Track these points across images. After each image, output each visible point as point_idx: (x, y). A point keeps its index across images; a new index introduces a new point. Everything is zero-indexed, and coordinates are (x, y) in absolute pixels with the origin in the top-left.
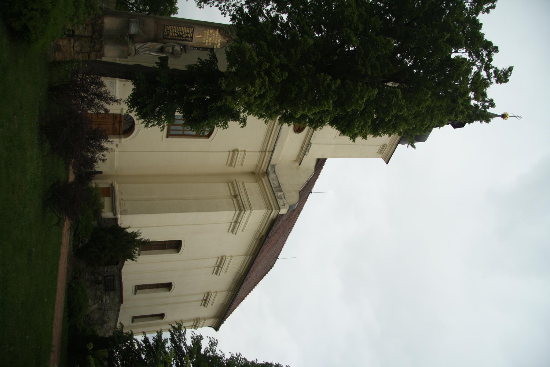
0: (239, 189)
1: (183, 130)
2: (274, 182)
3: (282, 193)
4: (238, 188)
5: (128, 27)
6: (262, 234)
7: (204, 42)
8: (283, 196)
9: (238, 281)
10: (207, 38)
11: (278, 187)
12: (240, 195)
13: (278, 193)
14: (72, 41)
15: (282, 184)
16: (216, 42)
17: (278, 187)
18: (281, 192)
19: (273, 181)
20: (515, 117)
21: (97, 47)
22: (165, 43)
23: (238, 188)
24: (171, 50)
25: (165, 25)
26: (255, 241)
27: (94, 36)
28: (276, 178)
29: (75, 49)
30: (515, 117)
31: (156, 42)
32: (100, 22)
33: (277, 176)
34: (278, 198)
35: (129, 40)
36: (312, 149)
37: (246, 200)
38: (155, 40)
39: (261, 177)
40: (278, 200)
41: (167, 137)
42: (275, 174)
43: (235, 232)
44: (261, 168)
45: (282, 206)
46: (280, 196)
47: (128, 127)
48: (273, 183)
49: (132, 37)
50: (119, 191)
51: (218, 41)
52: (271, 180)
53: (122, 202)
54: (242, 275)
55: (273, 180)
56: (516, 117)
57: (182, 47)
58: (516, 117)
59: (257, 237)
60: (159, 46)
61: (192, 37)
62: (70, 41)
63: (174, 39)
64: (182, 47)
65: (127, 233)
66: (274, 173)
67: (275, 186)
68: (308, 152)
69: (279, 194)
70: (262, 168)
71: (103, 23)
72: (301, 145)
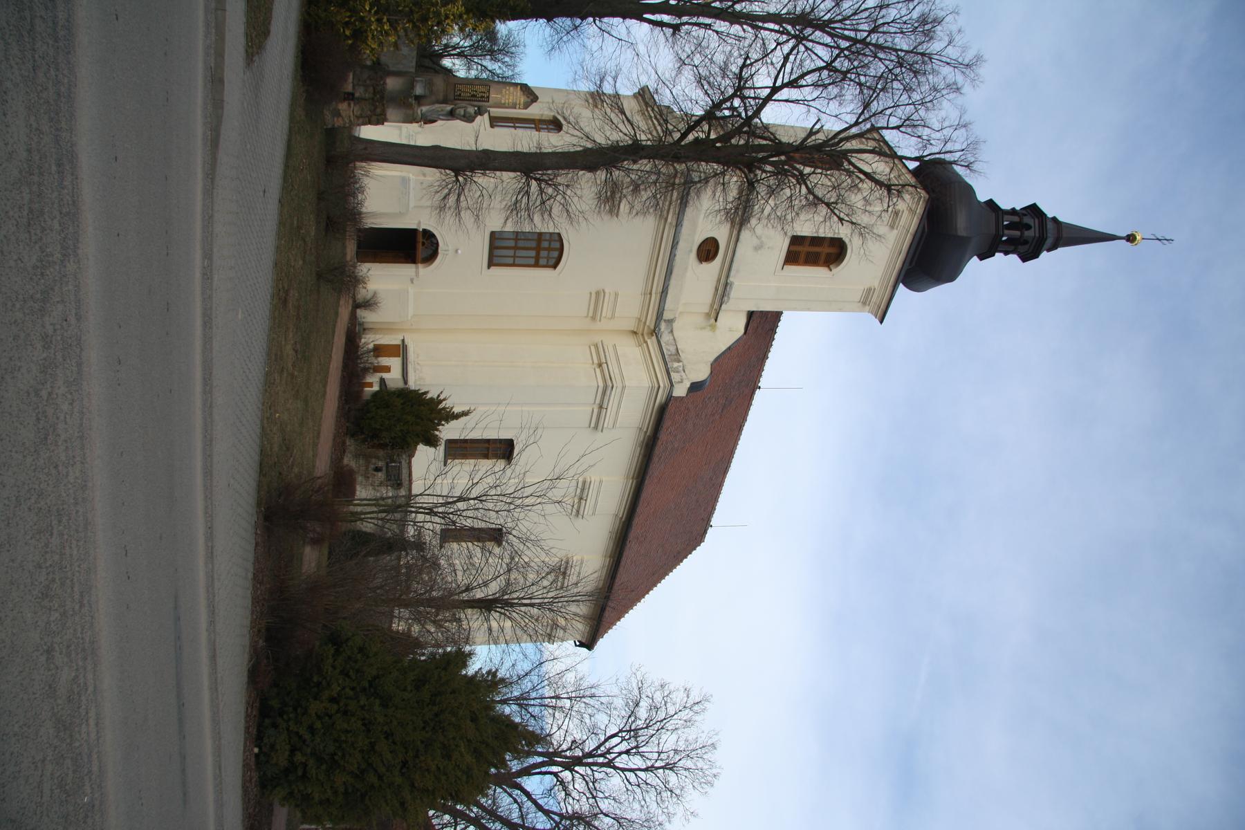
0: (607, 354)
1: (514, 257)
2: (669, 348)
3: (681, 364)
4: (604, 352)
5: (412, 87)
6: (648, 434)
7: (503, 102)
8: (681, 369)
9: (618, 535)
10: (507, 97)
11: (674, 355)
12: (606, 363)
13: (674, 363)
14: (352, 105)
15: (682, 352)
16: (518, 102)
17: (674, 355)
18: (678, 362)
19: (667, 346)
20: (1158, 239)
21: (378, 111)
22: (455, 105)
23: (604, 352)
24: (462, 113)
25: (455, 84)
26: (639, 449)
27: (376, 99)
28: (673, 341)
29: (355, 113)
30: (1158, 239)
31: (447, 103)
32: (382, 83)
33: (675, 339)
34: (672, 371)
35: (414, 102)
36: (734, 293)
37: (616, 371)
38: (445, 101)
39: (646, 338)
40: (672, 374)
41: (489, 266)
42: (673, 335)
43: (600, 427)
44: (645, 323)
45: (679, 382)
46: (677, 368)
47: (431, 252)
48: (667, 349)
49: (419, 99)
50: (414, 352)
51: (520, 101)
52: (663, 345)
53: (418, 367)
54: (623, 520)
55: (667, 344)
56: (1160, 240)
57: (476, 108)
58: (1160, 240)
59: (642, 439)
60: (449, 108)
61: (488, 97)
62: (349, 105)
63: (467, 100)
64: (476, 108)
65: (427, 400)
66: (670, 335)
67: (670, 353)
68: (729, 298)
69: (676, 365)
70: (647, 324)
71: (385, 83)
72: (714, 286)
